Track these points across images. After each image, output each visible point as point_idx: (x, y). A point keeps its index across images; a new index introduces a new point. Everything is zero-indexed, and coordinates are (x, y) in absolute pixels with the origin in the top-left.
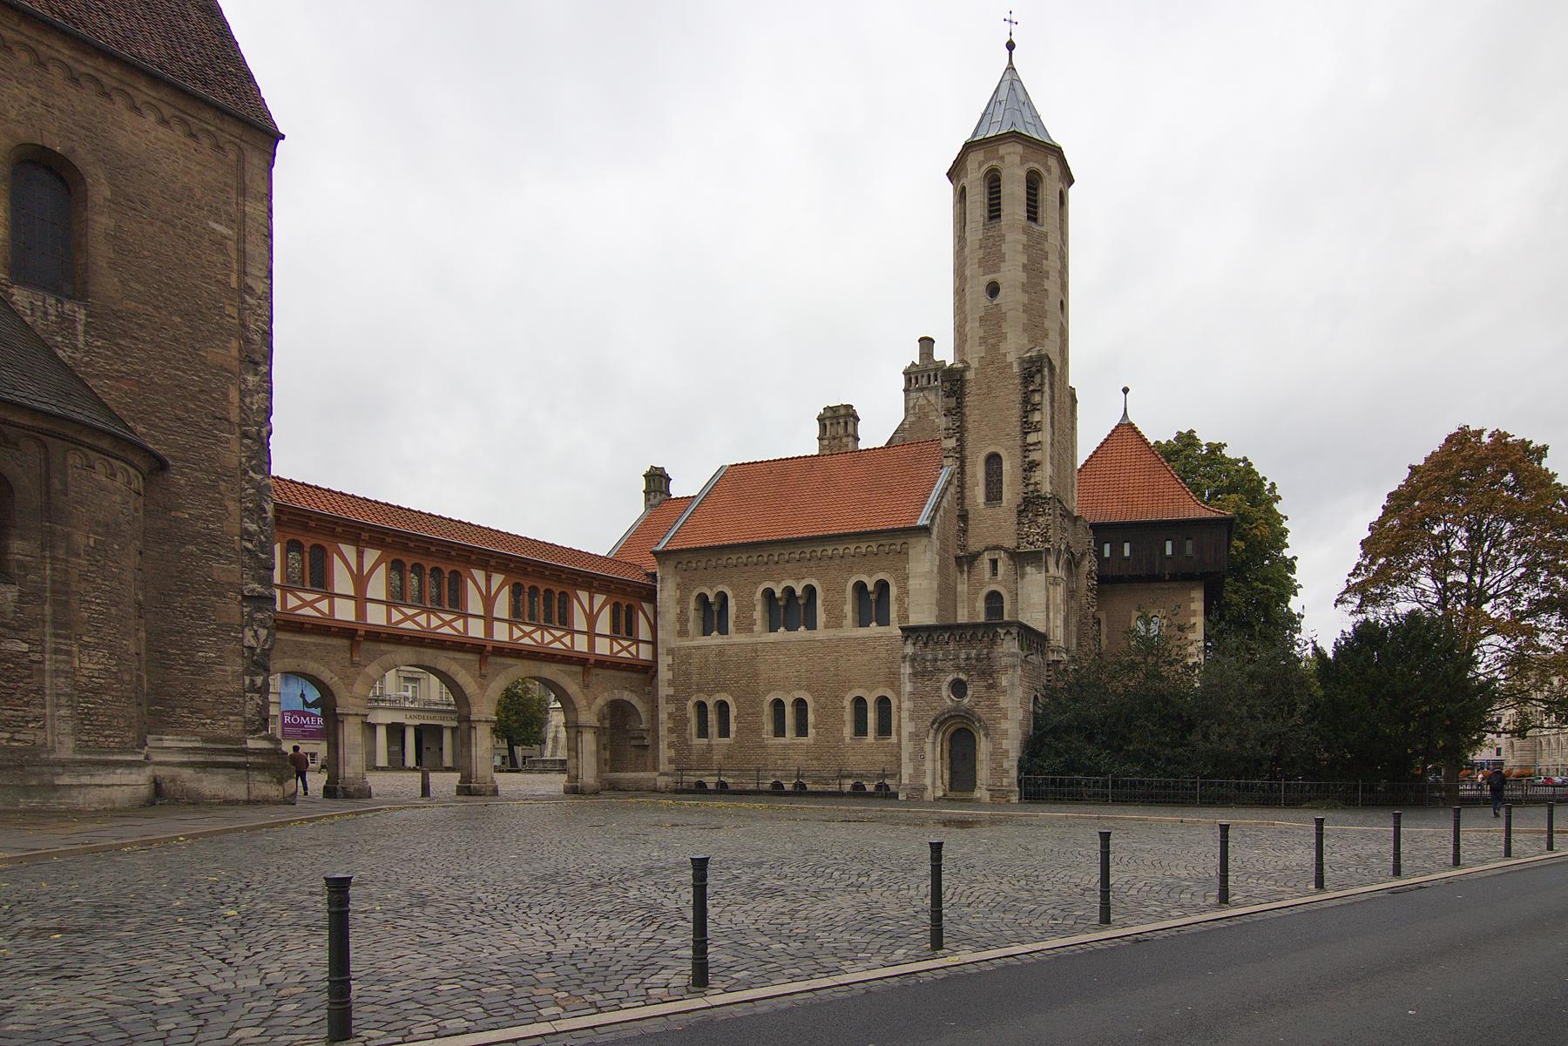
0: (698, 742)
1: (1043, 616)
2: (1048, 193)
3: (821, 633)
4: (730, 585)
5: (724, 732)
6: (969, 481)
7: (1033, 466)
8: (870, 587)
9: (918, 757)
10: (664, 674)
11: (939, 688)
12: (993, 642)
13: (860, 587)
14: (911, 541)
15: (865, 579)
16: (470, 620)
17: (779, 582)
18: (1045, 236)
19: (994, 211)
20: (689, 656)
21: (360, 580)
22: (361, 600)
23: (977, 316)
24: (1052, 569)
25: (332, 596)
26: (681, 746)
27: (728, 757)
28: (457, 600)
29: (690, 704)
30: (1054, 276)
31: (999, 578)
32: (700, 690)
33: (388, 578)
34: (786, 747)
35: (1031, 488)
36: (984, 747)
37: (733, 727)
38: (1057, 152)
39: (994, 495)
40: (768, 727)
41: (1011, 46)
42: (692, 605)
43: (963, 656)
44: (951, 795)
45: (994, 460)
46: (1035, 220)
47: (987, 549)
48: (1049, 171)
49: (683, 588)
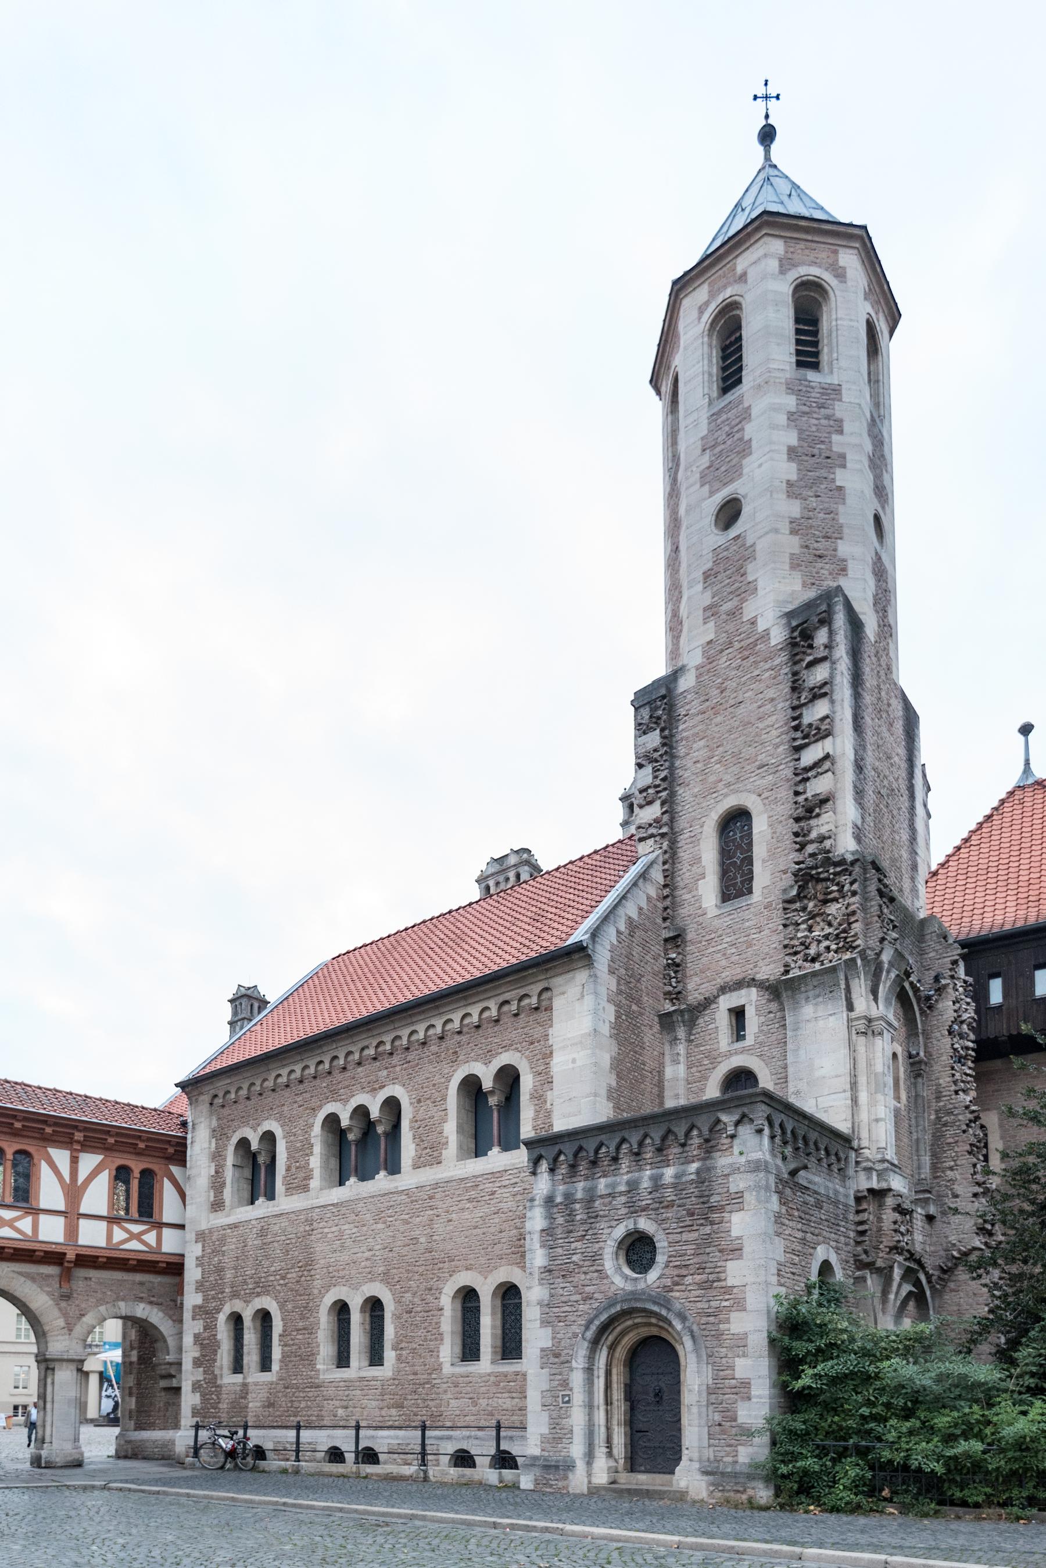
0: (229, 1380)
1: (843, 1101)
2: (846, 313)
3: (409, 1178)
4: (281, 1118)
5: (265, 1365)
6: (685, 874)
7: (810, 810)
8: (487, 1084)
9: (558, 1401)
10: (192, 1273)
11: (595, 1258)
12: (709, 1147)
13: (471, 1087)
14: (557, 982)
15: (478, 1069)
16: (42, 1217)
17: (345, 1101)
18: (834, 392)
19: (730, 372)
20: (223, 1240)
21: (74, 1192)
22: (72, 1215)
23: (699, 575)
24: (862, 1004)
25: (35, 1212)
26: (209, 1388)
27: (270, 1404)
28: (27, 1191)
29: (222, 1317)
30: (858, 461)
31: (750, 1040)
32: (235, 1295)
33: (113, 1192)
34: (349, 1384)
35: (810, 849)
36: (694, 1378)
37: (277, 1353)
38: (858, 237)
39: (735, 881)
40: (325, 1349)
41: (767, 135)
42: (230, 1159)
43: (646, 1184)
44: (627, 1480)
45: (735, 823)
46: (815, 366)
47: (724, 989)
48: (841, 275)
49: (219, 1134)
